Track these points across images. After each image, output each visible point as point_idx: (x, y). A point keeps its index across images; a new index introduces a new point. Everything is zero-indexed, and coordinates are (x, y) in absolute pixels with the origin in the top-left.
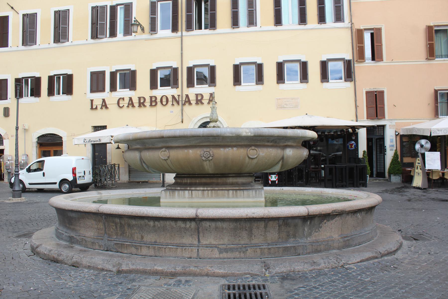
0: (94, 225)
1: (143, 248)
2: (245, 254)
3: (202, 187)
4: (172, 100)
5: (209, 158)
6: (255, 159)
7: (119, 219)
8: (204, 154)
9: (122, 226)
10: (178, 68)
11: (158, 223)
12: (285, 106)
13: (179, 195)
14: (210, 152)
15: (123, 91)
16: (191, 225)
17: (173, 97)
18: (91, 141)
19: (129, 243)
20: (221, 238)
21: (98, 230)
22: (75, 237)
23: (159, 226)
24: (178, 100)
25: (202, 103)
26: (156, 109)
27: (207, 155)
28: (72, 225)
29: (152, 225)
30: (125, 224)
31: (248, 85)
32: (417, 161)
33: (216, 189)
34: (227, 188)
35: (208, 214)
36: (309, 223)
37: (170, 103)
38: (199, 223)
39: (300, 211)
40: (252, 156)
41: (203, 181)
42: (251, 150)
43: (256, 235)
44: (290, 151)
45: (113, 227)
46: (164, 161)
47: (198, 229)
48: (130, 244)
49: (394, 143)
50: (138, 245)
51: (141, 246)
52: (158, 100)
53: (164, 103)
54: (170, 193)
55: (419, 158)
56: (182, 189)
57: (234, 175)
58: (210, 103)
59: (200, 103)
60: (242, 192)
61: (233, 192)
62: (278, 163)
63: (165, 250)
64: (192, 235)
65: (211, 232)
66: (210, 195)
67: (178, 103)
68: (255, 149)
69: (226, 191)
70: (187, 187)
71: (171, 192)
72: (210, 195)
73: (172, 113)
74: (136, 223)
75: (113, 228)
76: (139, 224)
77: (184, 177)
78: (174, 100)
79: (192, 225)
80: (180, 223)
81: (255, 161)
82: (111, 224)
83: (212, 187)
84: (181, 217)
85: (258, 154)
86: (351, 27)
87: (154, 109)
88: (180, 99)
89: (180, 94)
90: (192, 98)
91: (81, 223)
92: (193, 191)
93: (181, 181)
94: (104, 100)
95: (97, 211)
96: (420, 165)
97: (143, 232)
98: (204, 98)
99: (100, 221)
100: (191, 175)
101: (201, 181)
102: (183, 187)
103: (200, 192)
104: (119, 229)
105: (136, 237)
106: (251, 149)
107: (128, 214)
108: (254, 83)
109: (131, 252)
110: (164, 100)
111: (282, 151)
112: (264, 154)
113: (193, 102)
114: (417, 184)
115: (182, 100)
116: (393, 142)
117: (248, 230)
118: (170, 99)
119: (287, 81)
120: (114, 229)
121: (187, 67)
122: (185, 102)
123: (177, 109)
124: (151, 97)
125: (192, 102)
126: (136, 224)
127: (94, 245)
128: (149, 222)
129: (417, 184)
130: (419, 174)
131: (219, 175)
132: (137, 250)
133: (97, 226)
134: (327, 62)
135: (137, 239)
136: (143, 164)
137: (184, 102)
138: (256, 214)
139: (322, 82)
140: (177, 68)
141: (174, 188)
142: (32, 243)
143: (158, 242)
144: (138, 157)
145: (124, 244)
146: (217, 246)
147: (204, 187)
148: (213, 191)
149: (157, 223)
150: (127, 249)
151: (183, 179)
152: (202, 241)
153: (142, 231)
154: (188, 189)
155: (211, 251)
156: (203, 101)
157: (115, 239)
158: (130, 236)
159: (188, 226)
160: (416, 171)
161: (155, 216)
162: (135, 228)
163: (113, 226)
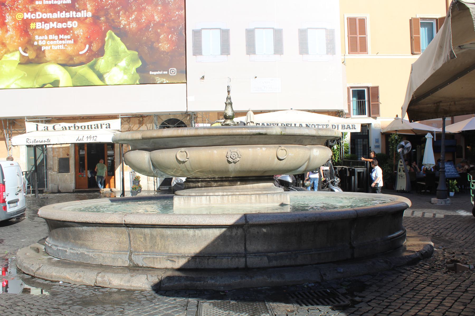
0: (114, 238)
3: (221, 192)
11: (199, 232)
18: (36, 141)
20: (269, 245)
21: (120, 243)
22: (86, 253)
23: (200, 235)
27: (234, 156)
28: (80, 240)
29: (192, 235)
30: (157, 235)
32: (400, 163)
36: (355, 226)
39: (349, 213)
44: (317, 151)
45: (140, 239)
49: (380, 143)
54: (184, 200)
55: (401, 160)
56: (197, 194)
60: (265, 196)
61: (256, 196)
65: (259, 240)
70: (204, 192)
74: (172, 233)
75: (140, 241)
76: (176, 234)
79: (239, 233)
82: (137, 236)
91: (95, 237)
92: (211, 197)
96: (402, 167)
97: (180, 243)
102: (198, 193)
104: (148, 241)
112: (293, 155)
114: (401, 187)
116: (378, 142)
120: (141, 242)
126: (171, 234)
127: (116, 261)
129: (401, 187)
130: (402, 177)
132: (174, 263)
138: (308, 217)
146: (266, 254)
147: (224, 192)
148: (234, 197)
150: (160, 263)
153: (178, 242)
154: (205, 194)
155: (260, 260)
157: (144, 253)
159: (234, 234)
160: (399, 173)
162: (170, 239)
163: (141, 238)
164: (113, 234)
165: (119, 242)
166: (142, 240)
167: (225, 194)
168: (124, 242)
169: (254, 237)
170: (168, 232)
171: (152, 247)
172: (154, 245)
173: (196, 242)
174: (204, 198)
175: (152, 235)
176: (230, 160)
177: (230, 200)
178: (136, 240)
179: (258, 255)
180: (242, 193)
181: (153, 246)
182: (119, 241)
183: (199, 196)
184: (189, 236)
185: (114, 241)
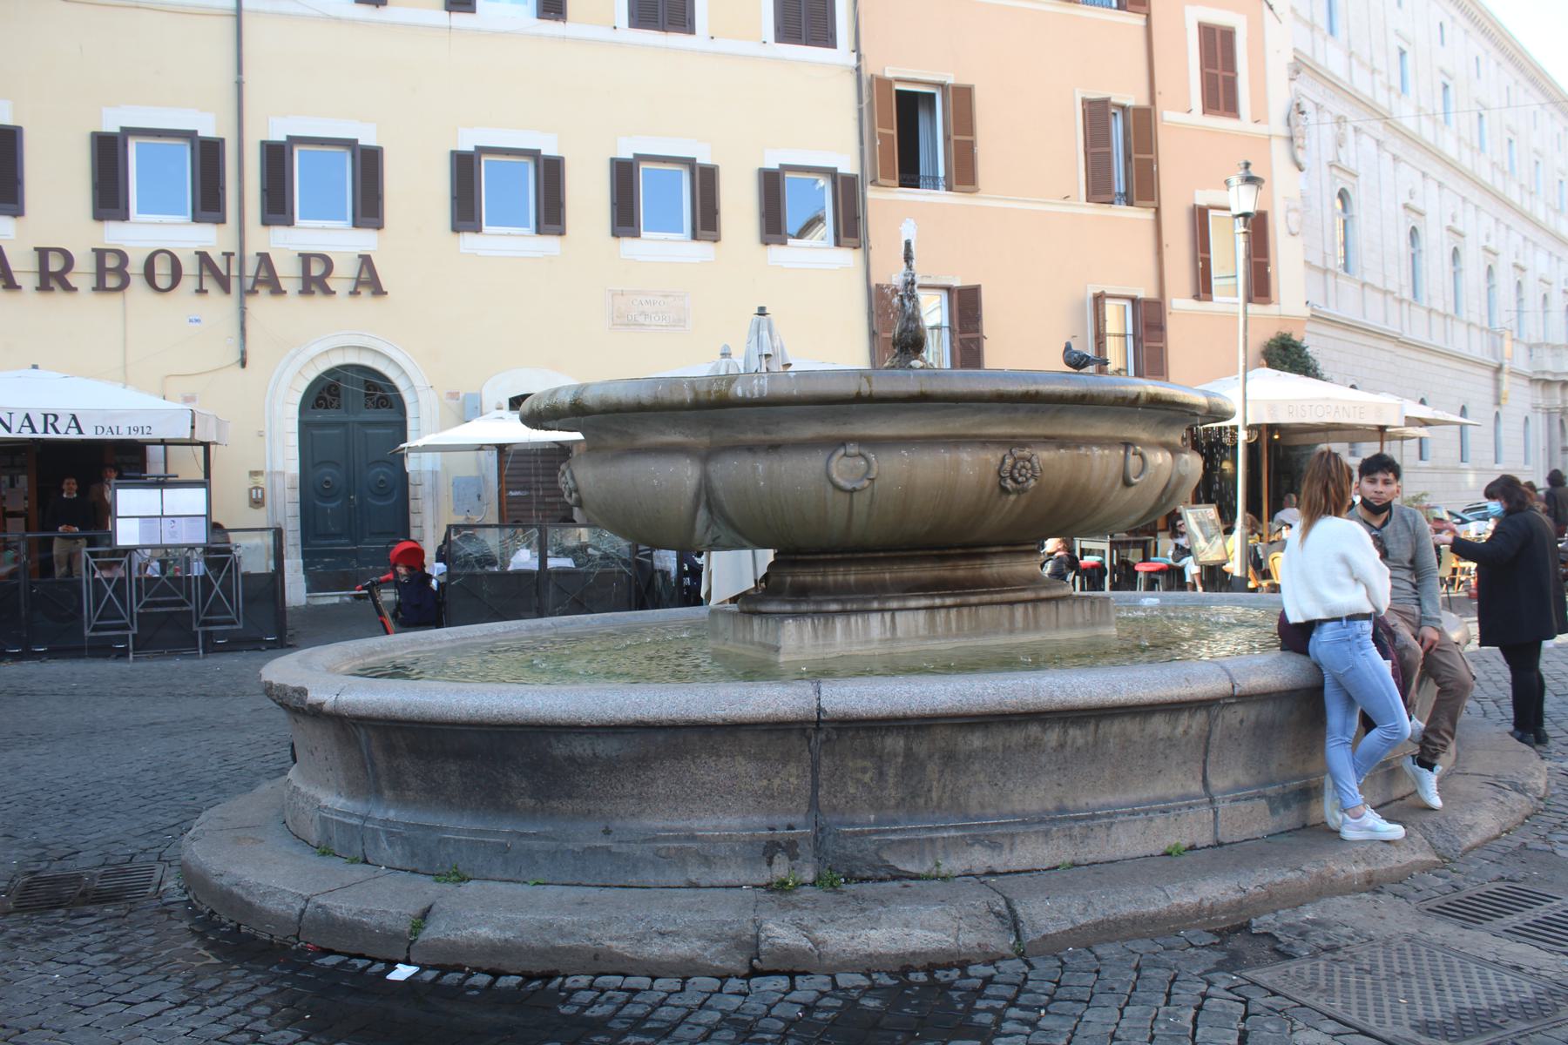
1: (1022, 842)
4: (198, 273)
7: (907, 737)
8: (1014, 467)
9: (911, 762)
10: (223, 140)
11: (1078, 732)
12: (641, 319)
13: (847, 631)
14: (1034, 459)
15: (161, 223)
16: (1190, 726)
17: (204, 258)
19: (953, 833)
21: (772, 797)
23: (1080, 742)
24: (224, 272)
25: (328, 292)
26: (124, 303)
30: (930, 756)
31: (157, 221)
33: (973, 599)
37: (189, 283)
41: (906, 575)
45: (859, 775)
48: (966, 833)
50: (999, 833)
51: (1013, 835)
52: (135, 267)
53: (163, 281)
54: (815, 629)
56: (849, 607)
58: (257, 292)
59: (318, 293)
61: (1026, 609)
63: (1108, 836)
66: (954, 625)
67: (224, 284)
69: (1005, 609)
71: (820, 622)
72: (954, 625)
73: (197, 324)
75: (858, 781)
77: (835, 563)
78: (206, 273)
79: (1194, 726)
82: (850, 764)
84: (1188, 698)
86: (858, 69)
87: (113, 301)
88: (234, 272)
89: (232, 247)
90: (287, 270)
92: (898, 615)
93: (820, 578)
94: (366, 261)
97: (1009, 779)
98: (336, 272)
99: (785, 759)
101: (899, 575)
103: (921, 615)
104: (891, 781)
105: (973, 803)
106: (845, 455)
107: (983, 710)
108: (345, 220)
109: (967, 867)
110: (162, 269)
111: (1386, 452)
113: (291, 284)
115: (241, 276)
118: (190, 267)
119: (301, 218)
121: (263, 143)
122: (257, 281)
123: (219, 307)
124: (100, 254)
125: (284, 284)
133: (765, 782)
134: (634, 164)
135: (982, 806)
137: (249, 283)
139: (456, 229)
140: (218, 143)
143: (1071, 808)
145: (932, 840)
148: (965, 611)
149: (1074, 732)
151: (830, 569)
152: (1212, 781)
153: (1004, 774)
154: (875, 605)
158: (946, 803)
159: (1180, 730)
161: (1100, 703)
162: (977, 767)
163: (864, 770)
165: (768, 793)
166: (867, 778)
167: (938, 602)
168: (788, 792)
169: (1230, 736)
171: (903, 799)
172: (911, 793)
173: (1065, 769)
174: (875, 619)
176: (1009, 484)
178: (841, 778)
179: (972, 820)
181: (908, 799)
182: (767, 788)
185: (744, 792)
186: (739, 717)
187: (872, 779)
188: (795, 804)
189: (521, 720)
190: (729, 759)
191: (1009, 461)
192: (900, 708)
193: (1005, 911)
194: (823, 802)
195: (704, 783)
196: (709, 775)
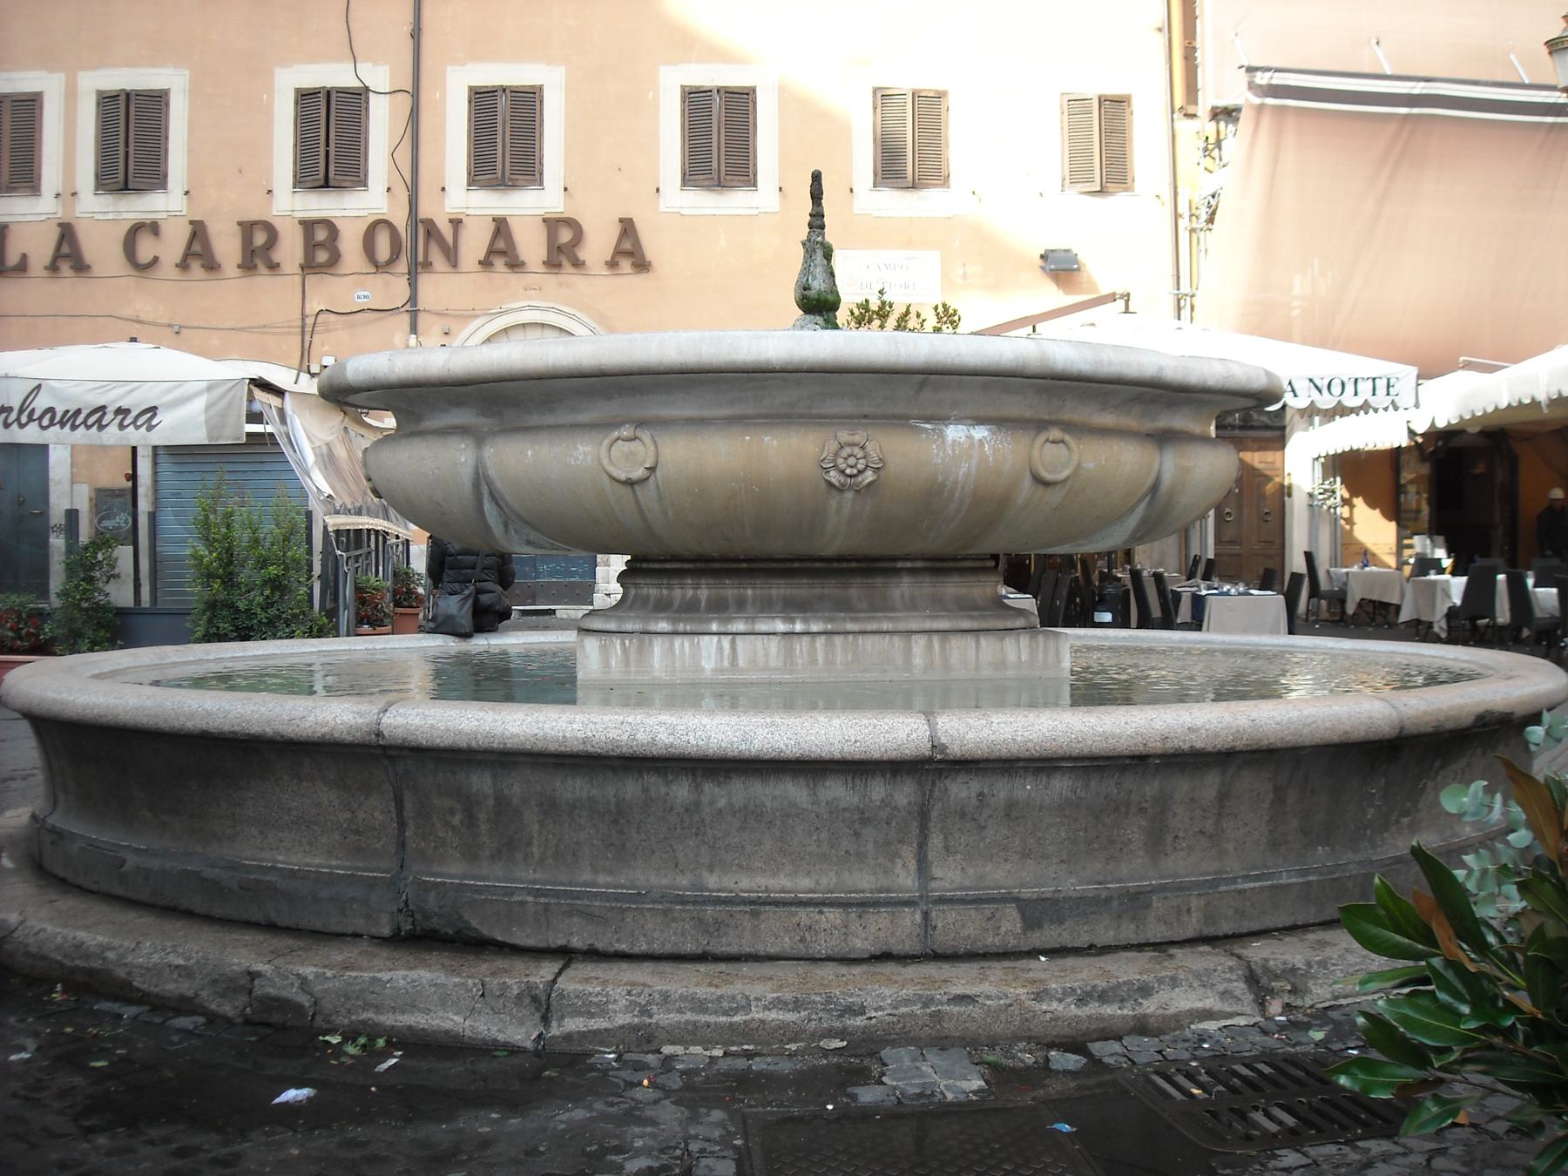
2: (1138, 927)
5: (860, 479)
6: (1058, 487)
8: (836, 454)
21: (357, 832)
25: (578, 264)
27: (852, 461)
33: (850, 626)
34: (901, 626)
35: (993, 737)
38: (933, 781)
40: (1047, 471)
42: (1048, 444)
43: (1181, 834)
46: (625, 492)
47: (923, 816)
56: (681, 627)
57: (919, 564)
59: (262, 269)
60: (969, 641)
61: (930, 642)
62: (1131, 510)
64: (888, 843)
68: (1063, 442)
69: (896, 639)
70: (710, 620)
77: (681, 573)
80: (836, 790)
81: (1055, 497)
83: (831, 620)
84: (857, 757)
85: (1074, 463)
92: (739, 638)
93: (665, 592)
95: (369, 733)
100: (714, 560)
103: (774, 644)
104: (484, 827)
107: (562, 748)
111: (1157, 455)
117: (1150, 810)
120: (454, 828)
128: (668, 784)
131: (854, 565)
133: (348, 815)
136: (488, 506)
138: (1203, 731)
141: (638, 626)
142: (950, 1019)
144: (467, 473)
148: (838, 640)
149: (709, 788)
152: (937, 872)
154: (714, 627)
156: (583, 254)
163: (452, 812)
164: (326, 795)
166: (456, 820)
167: (799, 627)
170: (573, 788)
175: (499, 799)
177: (820, 658)
180: (873, 626)
183: (688, 637)
184: (671, 809)
186: (296, 734)
187: (461, 822)
188: (382, 843)
189: (553, 748)
190: (310, 784)
191: (834, 446)
192: (464, 738)
193: (543, 998)
194: (412, 845)
195: (290, 809)
196: (293, 801)
